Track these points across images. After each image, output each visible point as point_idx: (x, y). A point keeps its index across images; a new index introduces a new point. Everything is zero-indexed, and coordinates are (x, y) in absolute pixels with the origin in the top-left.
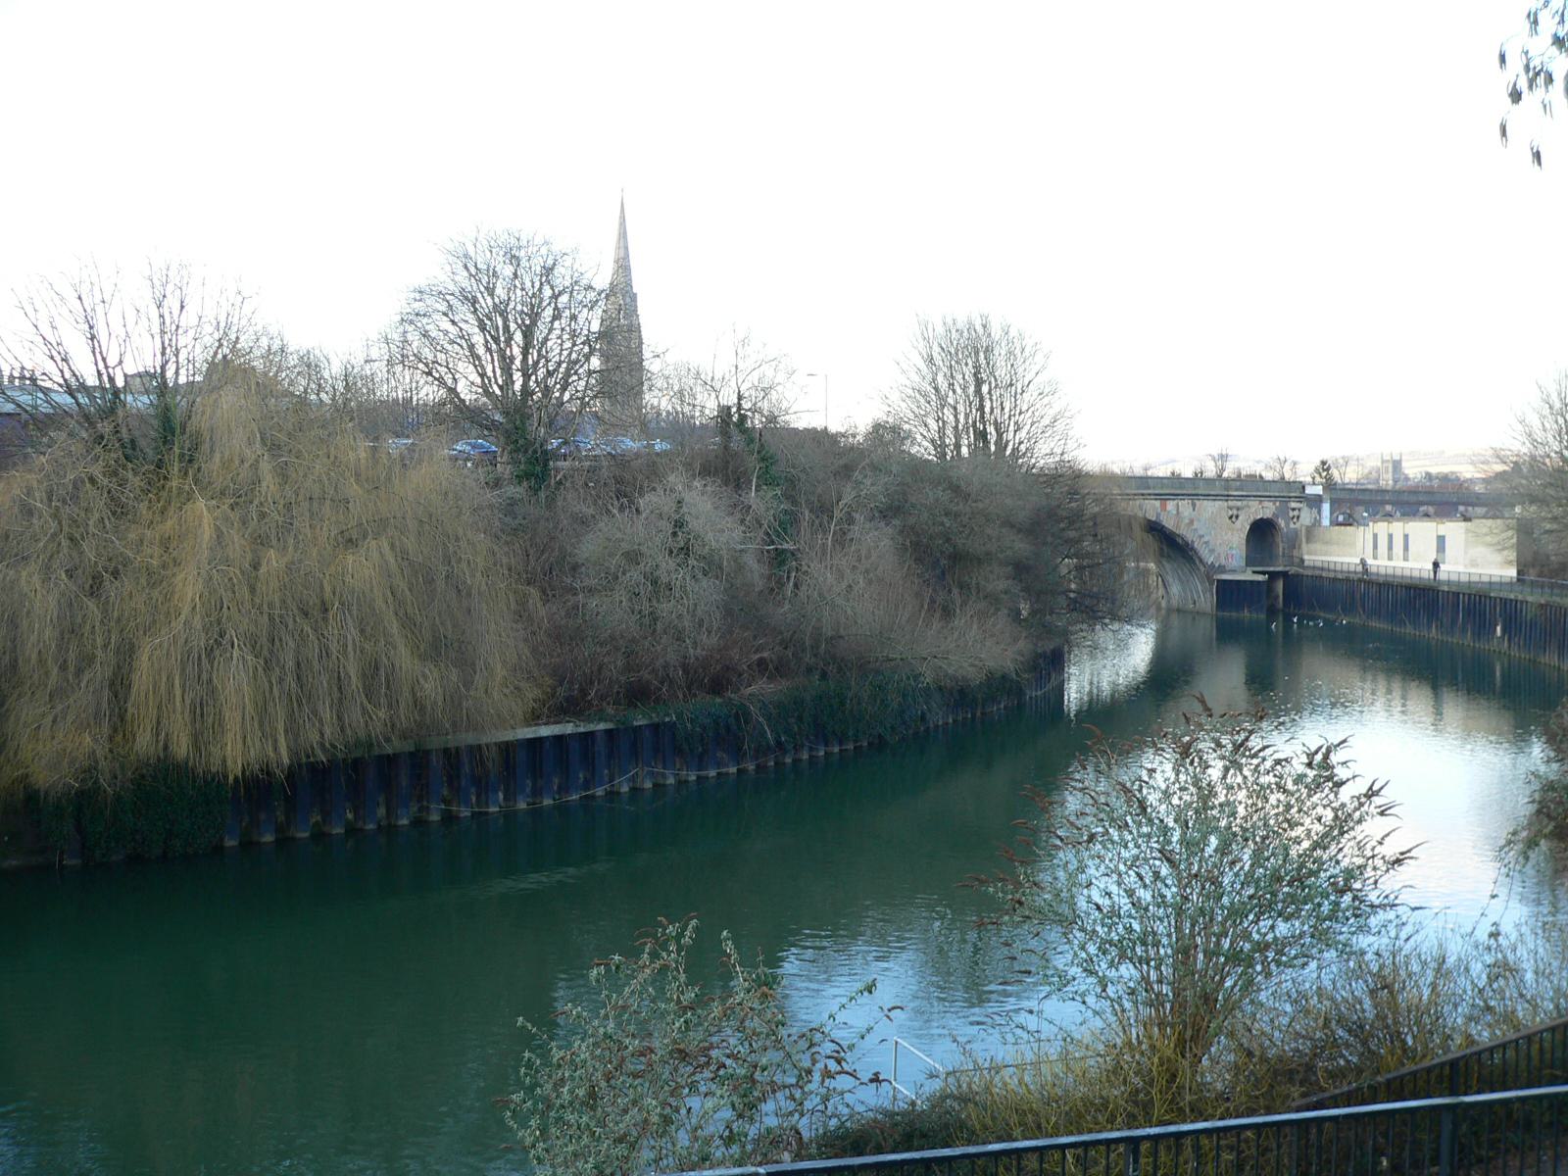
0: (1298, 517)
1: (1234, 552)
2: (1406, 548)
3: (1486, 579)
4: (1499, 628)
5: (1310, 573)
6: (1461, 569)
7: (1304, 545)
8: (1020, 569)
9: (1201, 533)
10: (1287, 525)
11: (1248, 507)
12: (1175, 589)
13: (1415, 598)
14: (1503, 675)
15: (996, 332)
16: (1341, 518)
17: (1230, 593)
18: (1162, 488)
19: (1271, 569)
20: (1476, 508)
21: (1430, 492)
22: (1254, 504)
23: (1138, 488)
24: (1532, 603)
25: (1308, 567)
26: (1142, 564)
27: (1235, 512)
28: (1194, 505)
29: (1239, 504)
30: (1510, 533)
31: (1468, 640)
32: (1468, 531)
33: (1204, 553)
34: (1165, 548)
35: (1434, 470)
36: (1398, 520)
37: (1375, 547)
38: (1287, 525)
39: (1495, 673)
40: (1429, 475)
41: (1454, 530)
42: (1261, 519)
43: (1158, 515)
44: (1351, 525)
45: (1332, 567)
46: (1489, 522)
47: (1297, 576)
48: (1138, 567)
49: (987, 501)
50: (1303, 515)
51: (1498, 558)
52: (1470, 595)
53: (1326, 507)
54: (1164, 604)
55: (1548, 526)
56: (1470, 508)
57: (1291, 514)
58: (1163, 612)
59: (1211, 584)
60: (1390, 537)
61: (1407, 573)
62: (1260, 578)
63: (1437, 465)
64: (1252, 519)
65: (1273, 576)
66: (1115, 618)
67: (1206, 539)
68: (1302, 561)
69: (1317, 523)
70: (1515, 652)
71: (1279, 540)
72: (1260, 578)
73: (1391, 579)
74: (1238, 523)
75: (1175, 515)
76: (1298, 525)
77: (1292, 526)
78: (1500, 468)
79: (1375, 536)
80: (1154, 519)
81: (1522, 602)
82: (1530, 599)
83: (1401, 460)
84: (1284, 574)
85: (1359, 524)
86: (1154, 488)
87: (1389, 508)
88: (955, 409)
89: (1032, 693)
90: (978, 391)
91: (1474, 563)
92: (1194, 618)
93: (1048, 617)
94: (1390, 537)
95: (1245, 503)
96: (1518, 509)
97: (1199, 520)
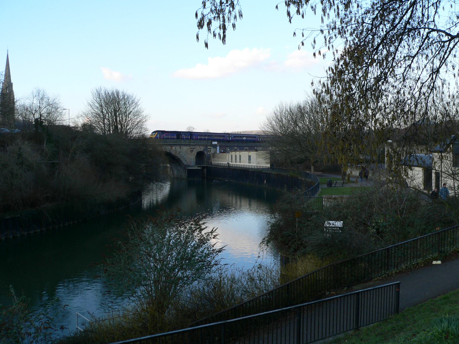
0: (210, 151)
2: (240, 159)
5: (214, 166)
6: (255, 165)
7: (212, 159)
9: (183, 155)
11: (196, 148)
12: (175, 172)
14: (266, 193)
16: (222, 151)
19: (203, 166)
22: (198, 147)
23: (164, 143)
25: (213, 165)
26: (165, 165)
27: (192, 149)
29: (193, 147)
30: (268, 155)
32: (257, 154)
41: (253, 154)
43: (170, 151)
44: (225, 153)
45: (220, 165)
50: (212, 150)
51: (264, 161)
53: (218, 148)
54: (172, 176)
55: (278, 153)
56: (258, 148)
60: (236, 156)
62: (199, 168)
65: (203, 168)
66: (157, 181)
67: (184, 157)
68: (212, 163)
69: (216, 152)
72: (199, 168)
74: (193, 153)
75: (175, 150)
76: (210, 153)
77: (209, 153)
79: (232, 156)
80: (169, 152)
82: (273, 173)
84: (207, 167)
87: (236, 148)
88: (109, 119)
90: (115, 114)
94: (236, 156)
96: (270, 148)
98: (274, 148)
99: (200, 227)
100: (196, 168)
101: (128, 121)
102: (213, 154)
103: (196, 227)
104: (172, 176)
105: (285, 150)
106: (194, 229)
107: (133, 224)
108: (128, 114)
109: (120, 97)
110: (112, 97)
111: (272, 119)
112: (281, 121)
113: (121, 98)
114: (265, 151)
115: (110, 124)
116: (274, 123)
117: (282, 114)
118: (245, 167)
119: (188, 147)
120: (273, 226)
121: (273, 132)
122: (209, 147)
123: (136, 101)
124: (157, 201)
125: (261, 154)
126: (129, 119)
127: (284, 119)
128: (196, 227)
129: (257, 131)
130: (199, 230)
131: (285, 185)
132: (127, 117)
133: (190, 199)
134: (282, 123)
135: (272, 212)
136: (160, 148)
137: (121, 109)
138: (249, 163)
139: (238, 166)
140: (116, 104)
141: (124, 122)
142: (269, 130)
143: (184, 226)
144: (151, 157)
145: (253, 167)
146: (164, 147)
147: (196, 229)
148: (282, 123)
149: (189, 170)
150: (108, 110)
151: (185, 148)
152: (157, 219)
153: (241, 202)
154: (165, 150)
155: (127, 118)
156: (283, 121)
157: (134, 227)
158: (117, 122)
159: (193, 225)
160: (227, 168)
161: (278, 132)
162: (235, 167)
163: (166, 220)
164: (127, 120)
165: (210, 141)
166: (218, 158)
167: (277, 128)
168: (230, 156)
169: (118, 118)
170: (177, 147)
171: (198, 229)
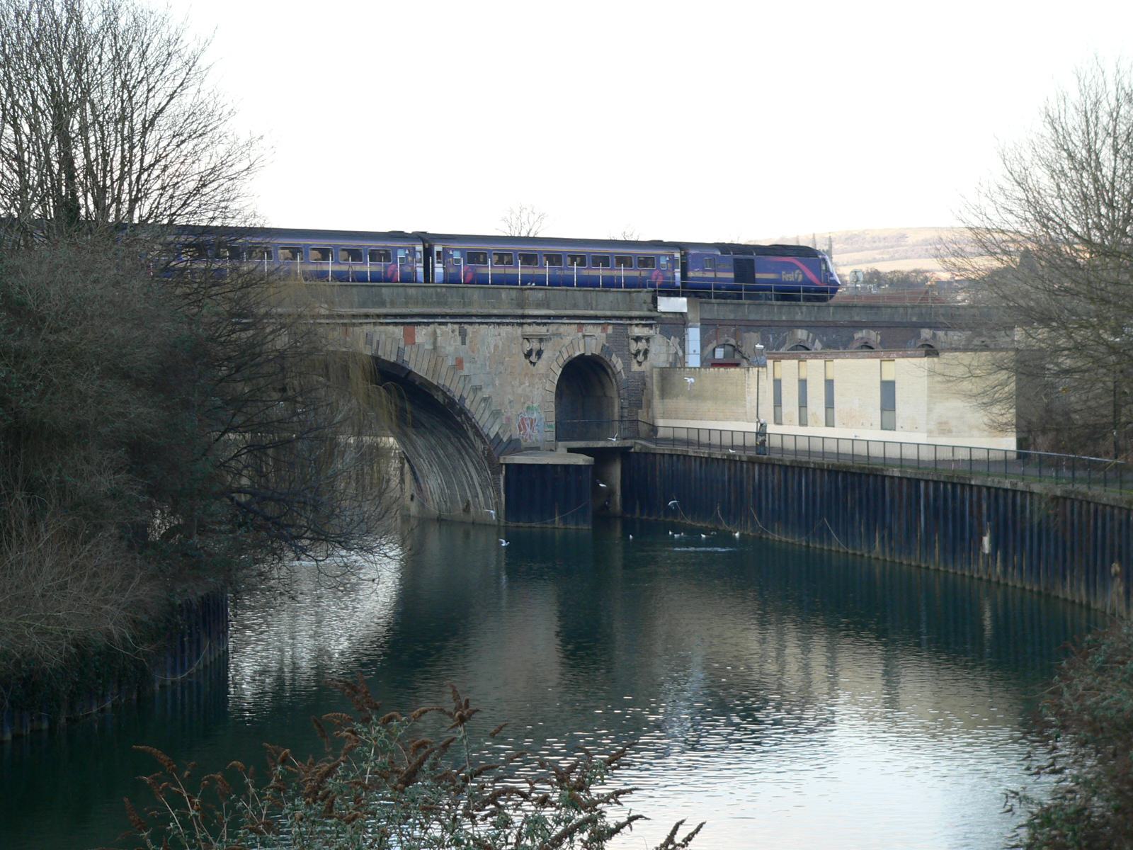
0: (646, 352)
1: (535, 415)
2: (830, 404)
3: (962, 455)
4: (986, 540)
5: (666, 449)
6: (922, 438)
7: (657, 403)
8: (140, 454)
9: (476, 382)
10: (627, 367)
11: (559, 335)
12: (434, 483)
13: (845, 488)
14: (995, 618)
15: (93, 22)
16: (720, 354)
17: (529, 488)
18: (406, 304)
19: (601, 444)
20: (951, 333)
21: (872, 306)
22: (569, 332)
23: (363, 305)
24: (1040, 495)
25: (666, 440)
26: (367, 439)
27: (535, 345)
28: (463, 334)
29: (542, 330)
30: (1003, 375)
31: (936, 561)
32: (932, 373)
33: (482, 417)
34: (408, 406)
35: (885, 268)
36: (816, 356)
37: (778, 402)
38: (627, 367)
39: (981, 620)
40: (875, 277)
41: (909, 371)
42: (582, 357)
43: (400, 352)
44: (737, 365)
45: (704, 438)
46: (967, 358)
47: (647, 455)
48: (359, 446)
49: (76, 331)
50: (654, 348)
51: (980, 417)
52: (936, 483)
53: (694, 334)
54: (414, 508)
55: (1067, 363)
56: (940, 334)
57: (634, 347)
58: (414, 523)
59: (496, 472)
60: (803, 383)
61: (831, 446)
62: (581, 460)
63: (892, 258)
64: (561, 362)
65: (602, 457)
66: (321, 536)
67: (486, 393)
68: (654, 429)
69: (678, 362)
70: (1014, 581)
71: (613, 393)
72: (581, 460)
73: (805, 459)
74: (542, 365)
75: (431, 351)
76: (645, 367)
77: (635, 367)
78: (986, 263)
79: (777, 383)
80: (393, 359)
81: (1023, 493)
82: (1036, 488)
83: (829, 252)
84: (623, 453)
85: (751, 364)
86: (393, 304)
87: (801, 334)
88: (19, 159)
89: (163, 678)
90: (61, 128)
91: (944, 428)
92: (467, 535)
93: (196, 539)
94: (803, 383)
95: (552, 328)
96: (1018, 334)
97: (473, 361)
98: (1043, 333)
99: (592, 821)
100: (560, 457)
101: (142, 170)
102: (666, 375)
103: (569, 820)
104: (414, 508)
105: (1112, 349)
106: (560, 829)
107: (178, 802)
108: (138, 126)
109: (85, 20)
110: (34, 18)
111: (1028, 156)
112: (1091, 163)
113: (96, 27)
114: (985, 356)
115: (25, 185)
116: (1042, 178)
117: (1092, 119)
118: (861, 449)
119: (509, 328)
120: (1044, 819)
121: (1034, 239)
122: (637, 331)
123: (188, 46)
124: (321, 652)
125: (960, 371)
126: (149, 159)
127: (1106, 154)
128: (569, 820)
129: (936, 229)
130: (585, 836)
131: (1116, 567)
132: (132, 147)
133: (521, 648)
134: (1096, 180)
135: (1034, 727)
136: (337, 334)
137: (95, 95)
138: (888, 425)
139: (817, 446)
140: (65, 66)
141: (116, 175)
142: (1013, 223)
143: (492, 814)
144: (284, 390)
145: (910, 453)
146: (361, 332)
147: (569, 833)
148: (1096, 180)
149: (516, 471)
150: (15, 103)
151: (490, 338)
152: (326, 767)
153: (832, 664)
154: (368, 352)
155: (137, 151)
156: (1099, 166)
157: (187, 823)
158: (71, 177)
159: (552, 804)
160: (751, 461)
161: (1070, 236)
162: (796, 452)
163: (383, 775)
164: (136, 166)
165: (645, 295)
166: (697, 396)
167: (1064, 209)
168: (767, 386)
169: (78, 153)
170: (440, 330)
171: (581, 826)
